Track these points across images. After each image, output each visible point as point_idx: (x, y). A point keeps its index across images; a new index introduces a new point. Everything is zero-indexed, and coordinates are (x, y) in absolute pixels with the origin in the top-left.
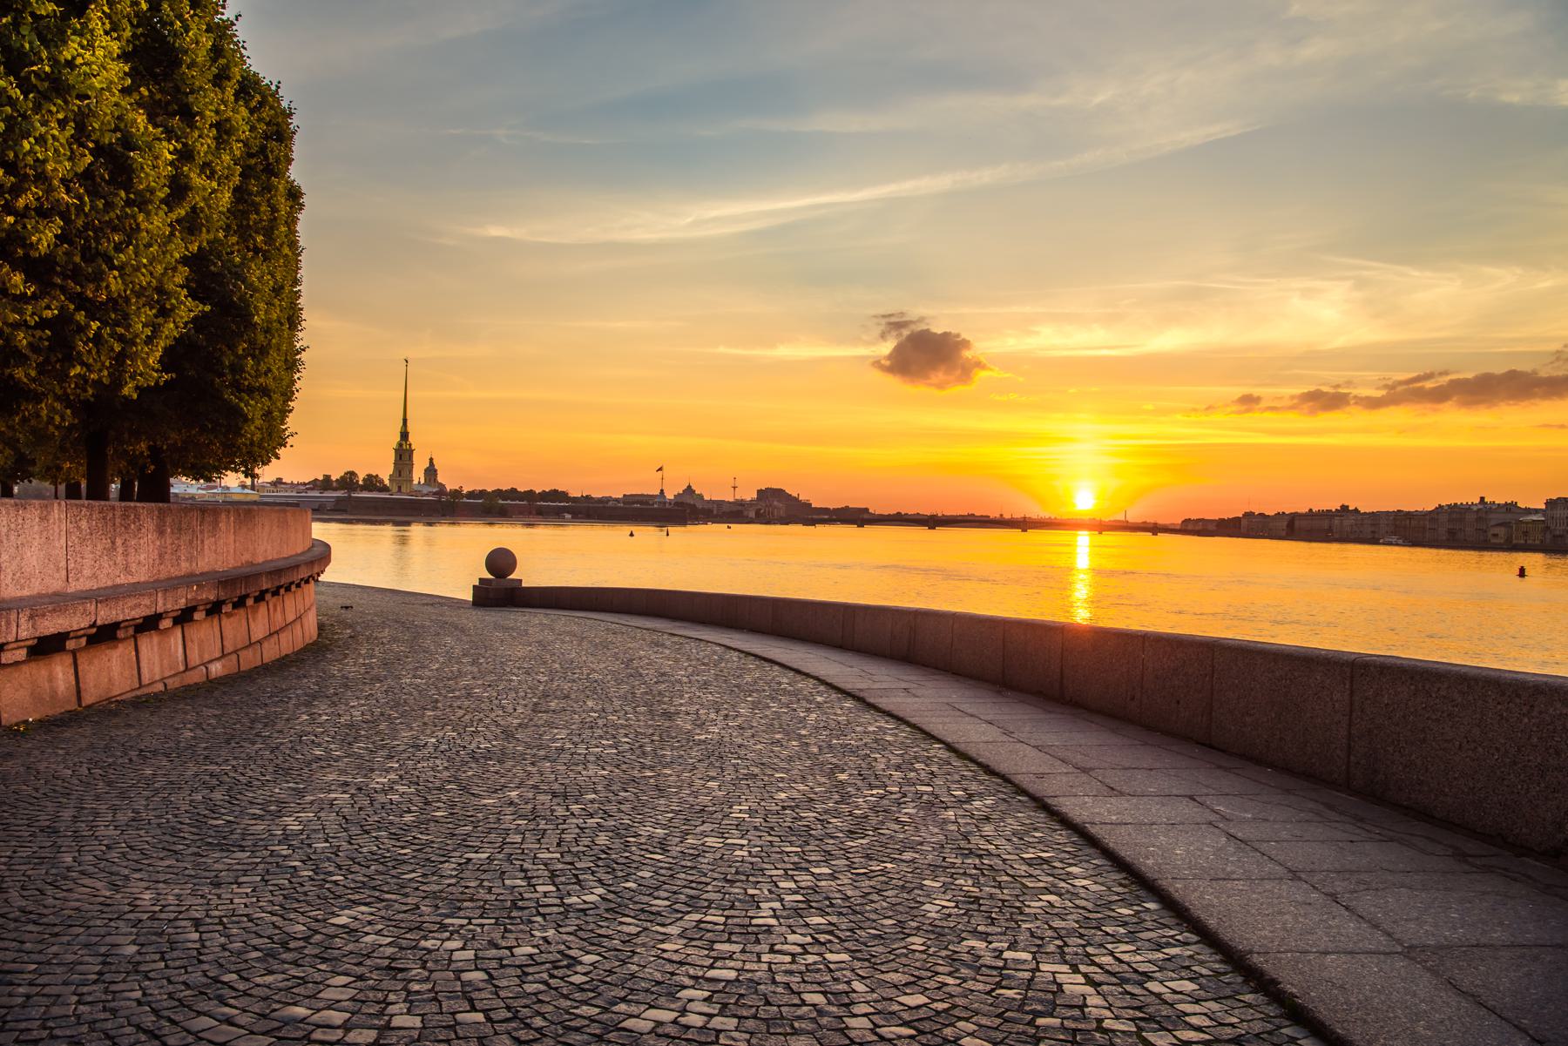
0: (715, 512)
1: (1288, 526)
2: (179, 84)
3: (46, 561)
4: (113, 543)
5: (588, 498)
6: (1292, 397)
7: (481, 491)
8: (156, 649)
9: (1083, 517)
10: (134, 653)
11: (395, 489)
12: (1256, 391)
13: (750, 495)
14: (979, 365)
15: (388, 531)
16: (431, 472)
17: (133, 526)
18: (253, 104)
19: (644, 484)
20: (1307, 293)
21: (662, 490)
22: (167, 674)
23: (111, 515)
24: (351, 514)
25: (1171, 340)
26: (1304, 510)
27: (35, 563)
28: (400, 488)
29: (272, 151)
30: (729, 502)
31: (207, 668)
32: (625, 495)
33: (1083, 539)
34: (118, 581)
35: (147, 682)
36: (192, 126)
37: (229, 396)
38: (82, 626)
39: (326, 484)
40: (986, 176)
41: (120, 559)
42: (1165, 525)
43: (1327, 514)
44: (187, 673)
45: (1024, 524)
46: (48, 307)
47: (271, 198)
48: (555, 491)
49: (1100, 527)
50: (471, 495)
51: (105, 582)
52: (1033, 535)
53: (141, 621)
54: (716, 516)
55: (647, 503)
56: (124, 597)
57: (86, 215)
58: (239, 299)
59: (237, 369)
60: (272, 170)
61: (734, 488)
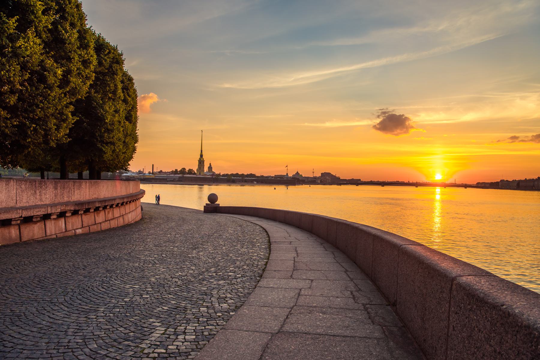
0: (306, 181)
1: (517, 185)
2: (65, 50)
3: (8, 197)
4: (35, 192)
5: (262, 176)
6: (533, 136)
7: (226, 174)
8: (53, 224)
9: (439, 182)
10: (44, 226)
11: (198, 174)
12: (517, 135)
13: (318, 175)
14: (412, 127)
15: (196, 187)
16: (210, 168)
17: (43, 187)
18: (106, 53)
19: (281, 171)
20: (522, 98)
21: (287, 174)
22: (57, 232)
23: (34, 183)
24: (184, 182)
25: (470, 117)
26: (523, 179)
27: (3, 198)
28: (200, 173)
29: (114, 67)
30: (311, 177)
31: (75, 231)
32: (275, 175)
33: (438, 190)
34: (37, 204)
35: (49, 235)
36: (71, 62)
37: (99, 145)
38: (16, 217)
39: (176, 172)
40: (398, 59)
41: (38, 197)
42: (470, 185)
43: (532, 180)
44: (66, 232)
45: (416, 185)
46: (15, 121)
47: (115, 82)
48: (251, 174)
49: (445, 185)
50: (223, 175)
51: (31, 203)
52: (420, 188)
53: (42, 216)
54: (306, 182)
55: (283, 178)
56: (33, 208)
57: (29, 92)
58: (101, 115)
59: (102, 137)
60: (115, 73)
61: (313, 172)
